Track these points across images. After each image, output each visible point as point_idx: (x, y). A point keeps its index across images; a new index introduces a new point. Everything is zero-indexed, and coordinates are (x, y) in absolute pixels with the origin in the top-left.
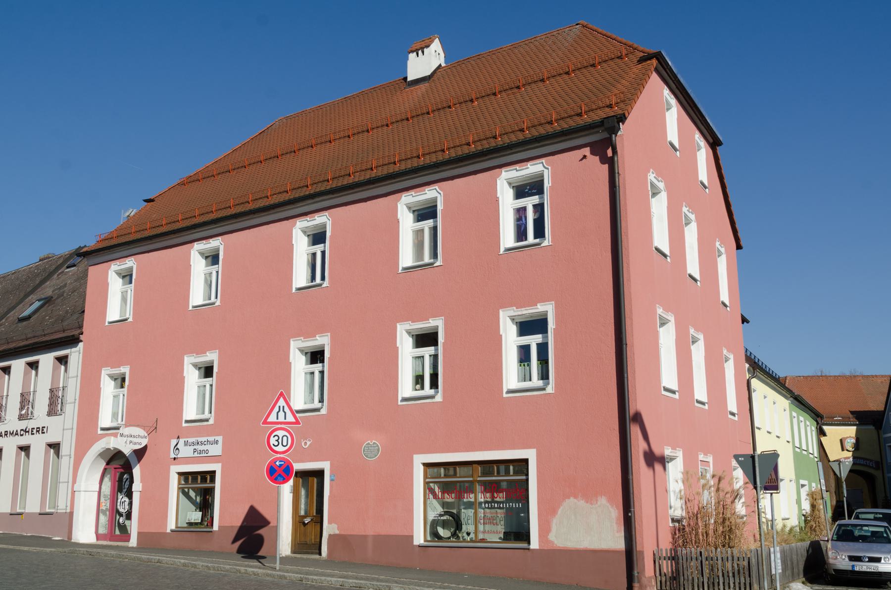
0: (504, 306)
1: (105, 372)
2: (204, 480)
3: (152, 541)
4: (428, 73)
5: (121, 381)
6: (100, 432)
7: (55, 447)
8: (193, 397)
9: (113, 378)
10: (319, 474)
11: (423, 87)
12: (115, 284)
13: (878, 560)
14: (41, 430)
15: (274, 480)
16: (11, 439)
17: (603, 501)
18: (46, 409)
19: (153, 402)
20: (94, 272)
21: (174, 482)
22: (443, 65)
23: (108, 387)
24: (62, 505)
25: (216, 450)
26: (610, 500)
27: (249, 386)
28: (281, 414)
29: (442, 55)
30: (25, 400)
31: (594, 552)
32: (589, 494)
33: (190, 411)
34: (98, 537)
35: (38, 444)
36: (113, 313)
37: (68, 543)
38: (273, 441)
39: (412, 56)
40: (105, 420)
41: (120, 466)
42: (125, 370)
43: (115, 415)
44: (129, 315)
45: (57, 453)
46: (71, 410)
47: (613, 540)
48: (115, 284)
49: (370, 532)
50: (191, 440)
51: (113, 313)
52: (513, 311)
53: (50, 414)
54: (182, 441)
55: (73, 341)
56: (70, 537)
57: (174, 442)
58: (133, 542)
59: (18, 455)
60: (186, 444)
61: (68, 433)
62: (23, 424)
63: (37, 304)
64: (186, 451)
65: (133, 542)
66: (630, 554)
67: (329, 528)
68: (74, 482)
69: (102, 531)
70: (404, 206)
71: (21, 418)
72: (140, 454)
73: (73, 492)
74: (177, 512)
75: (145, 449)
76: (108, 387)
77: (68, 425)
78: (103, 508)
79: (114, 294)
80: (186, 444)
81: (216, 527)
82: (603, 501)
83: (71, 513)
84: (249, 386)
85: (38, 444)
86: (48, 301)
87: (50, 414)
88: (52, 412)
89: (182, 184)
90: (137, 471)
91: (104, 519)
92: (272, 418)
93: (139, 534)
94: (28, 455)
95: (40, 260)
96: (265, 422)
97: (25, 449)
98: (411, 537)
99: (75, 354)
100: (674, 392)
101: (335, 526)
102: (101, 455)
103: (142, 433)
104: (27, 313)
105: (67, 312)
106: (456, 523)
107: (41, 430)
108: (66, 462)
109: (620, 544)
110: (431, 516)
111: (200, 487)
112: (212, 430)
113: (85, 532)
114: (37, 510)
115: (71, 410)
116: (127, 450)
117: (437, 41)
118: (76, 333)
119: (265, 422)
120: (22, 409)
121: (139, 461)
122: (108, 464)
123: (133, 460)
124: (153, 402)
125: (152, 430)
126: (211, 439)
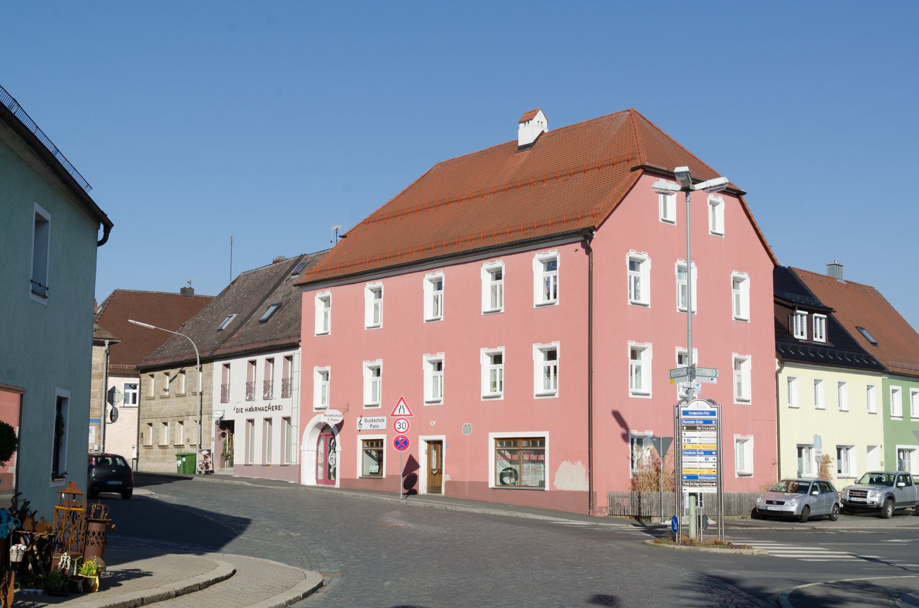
0: (535, 342)
1: (316, 369)
2: (377, 445)
3: (348, 484)
4: (532, 141)
5: (326, 375)
6: (315, 411)
7: (288, 419)
8: (371, 390)
9: (322, 373)
10: (440, 442)
11: (527, 152)
12: (320, 307)
13: (782, 503)
14: (278, 408)
15: (398, 448)
16: (259, 412)
17: (579, 463)
18: (281, 393)
19: (346, 391)
20: (306, 295)
21: (360, 445)
22: (546, 131)
23: (318, 379)
24: (294, 460)
25: (383, 426)
26: (583, 463)
27: (401, 386)
28: (402, 410)
29: (545, 122)
30: (267, 386)
31: (575, 492)
32: (573, 460)
33: (368, 399)
34: (318, 481)
35: (277, 416)
36: (319, 329)
37: (298, 485)
38: (397, 426)
39: (522, 125)
40: (317, 402)
41: (328, 433)
42: (328, 368)
43: (324, 399)
44: (329, 330)
45: (289, 423)
46: (296, 394)
47: (582, 486)
48: (320, 307)
49: (467, 480)
50: (369, 418)
51: (319, 329)
52: (540, 345)
53: (283, 396)
54: (363, 419)
55: (295, 346)
56: (300, 481)
57: (359, 419)
58: (337, 485)
59: (264, 424)
60: (366, 421)
61: (295, 410)
62: (266, 403)
63: (272, 309)
64: (366, 426)
65: (337, 485)
66: (591, 494)
67: (445, 477)
68: (300, 444)
69: (320, 477)
70: (485, 269)
71: (265, 399)
72: (339, 426)
73: (300, 451)
74: (362, 466)
75: (342, 422)
76: (318, 379)
77: (295, 405)
78: (320, 462)
79: (320, 311)
80: (366, 421)
81: (384, 476)
82: (579, 463)
83: (300, 465)
84: (401, 386)
85: (277, 416)
86: (279, 306)
87: (283, 396)
88: (284, 396)
89: (367, 222)
90: (338, 437)
91: (321, 469)
92: (397, 412)
93: (341, 479)
94: (271, 423)
95: (274, 262)
96: (392, 415)
97: (269, 420)
98: (487, 483)
99: (296, 354)
100: (648, 395)
101: (448, 476)
102: (317, 425)
103: (339, 413)
104: (265, 316)
105: (292, 319)
106: (515, 474)
107: (278, 408)
108: (295, 431)
109: (587, 489)
110: (500, 470)
111: (374, 448)
112: (380, 413)
113: (309, 478)
114: (261, 463)
115: (296, 394)
116: (332, 424)
117: (540, 113)
118: (296, 340)
119: (392, 415)
120: (265, 392)
121: (339, 431)
122: (322, 431)
123: (335, 431)
124: (346, 391)
125: (346, 411)
126: (380, 418)
